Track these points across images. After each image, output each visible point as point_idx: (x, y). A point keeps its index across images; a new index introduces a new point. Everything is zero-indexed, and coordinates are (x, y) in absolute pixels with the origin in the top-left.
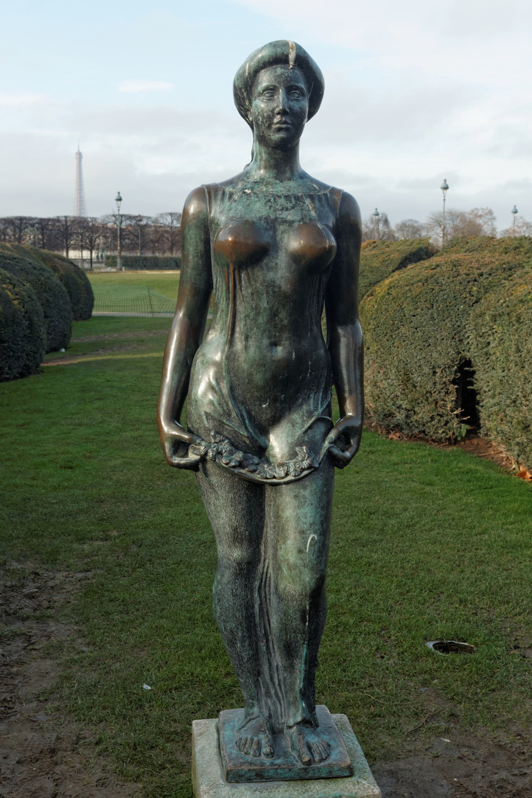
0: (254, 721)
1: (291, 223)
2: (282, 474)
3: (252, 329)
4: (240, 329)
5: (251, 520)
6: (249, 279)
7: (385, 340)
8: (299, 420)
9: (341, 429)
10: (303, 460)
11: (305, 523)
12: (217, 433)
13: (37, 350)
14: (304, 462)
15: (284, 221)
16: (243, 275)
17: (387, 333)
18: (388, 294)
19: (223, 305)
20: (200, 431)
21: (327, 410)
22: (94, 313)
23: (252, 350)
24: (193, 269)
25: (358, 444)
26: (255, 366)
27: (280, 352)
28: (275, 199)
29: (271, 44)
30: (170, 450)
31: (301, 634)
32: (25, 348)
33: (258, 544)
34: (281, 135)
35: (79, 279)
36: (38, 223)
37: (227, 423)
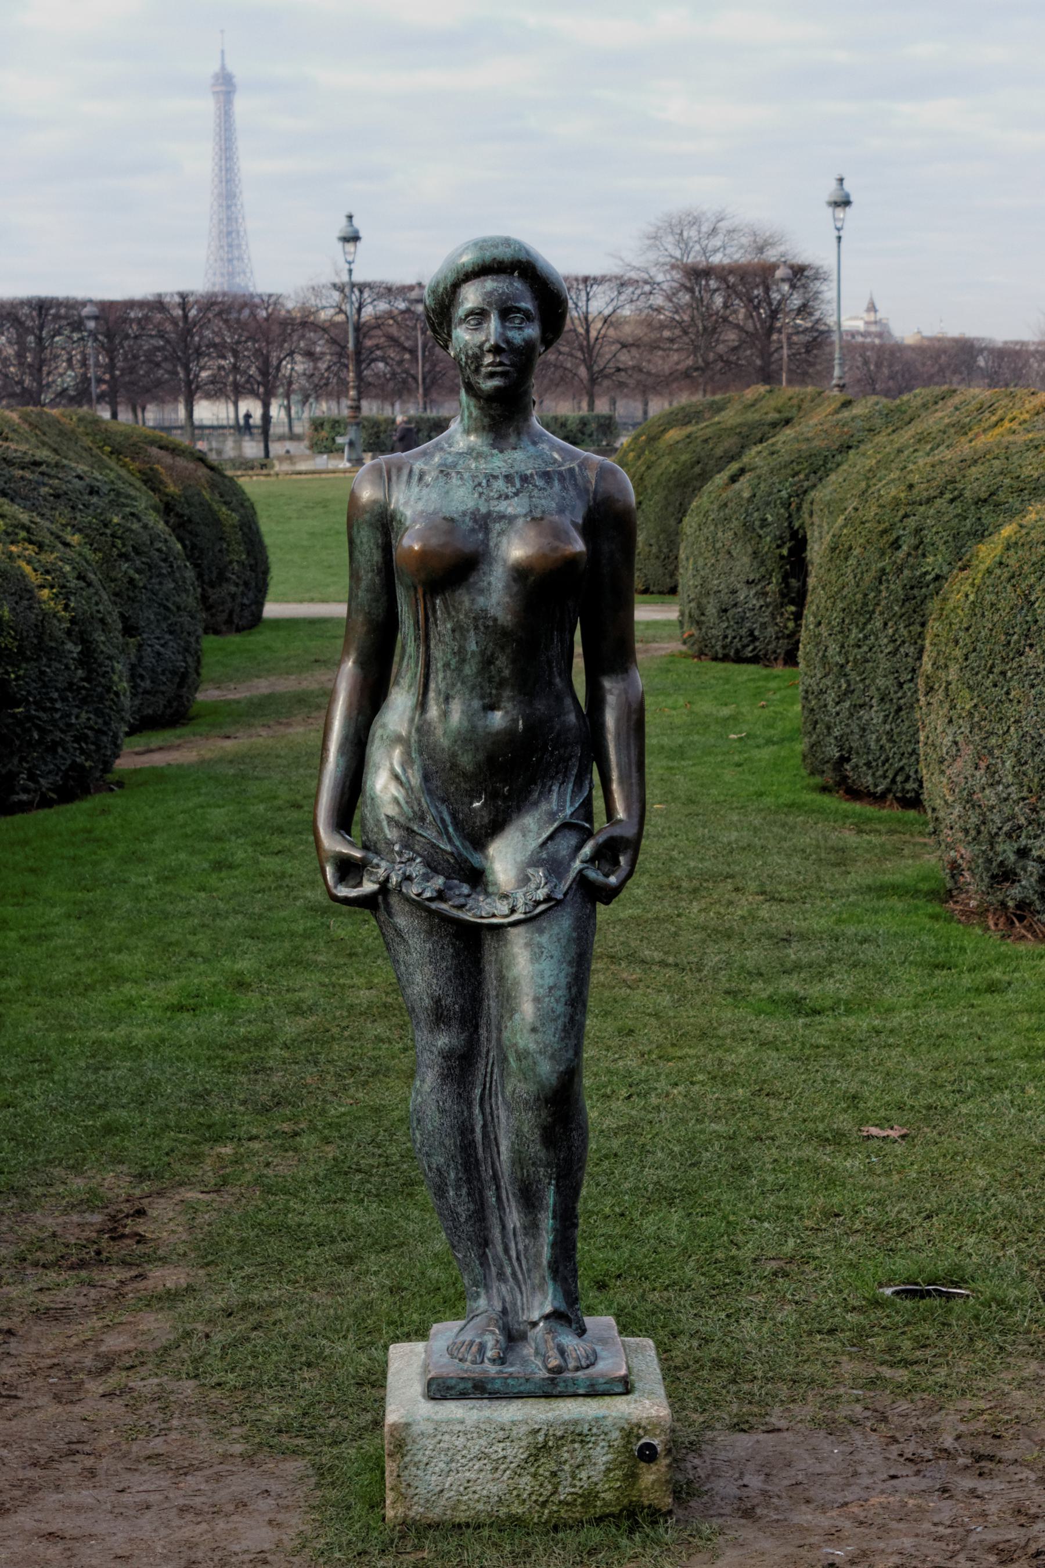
0: (479, 1319)
1: (511, 519)
2: (507, 912)
3: (454, 685)
5: (462, 985)
6: (446, 607)
7: (988, 683)
10: (538, 889)
11: (542, 986)
12: (406, 846)
13: (106, 723)
15: (502, 517)
17: (993, 666)
18: (1001, 563)
19: (411, 648)
21: (582, 811)
22: (271, 610)
23: (456, 717)
24: (367, 591)
27: (498, 719)
29: (475, 244)
30: (333, 876)
32: (73, 721)
33: (476, 1027)
34: (496, 382)
35: (224, 509)
36: (96, 318)
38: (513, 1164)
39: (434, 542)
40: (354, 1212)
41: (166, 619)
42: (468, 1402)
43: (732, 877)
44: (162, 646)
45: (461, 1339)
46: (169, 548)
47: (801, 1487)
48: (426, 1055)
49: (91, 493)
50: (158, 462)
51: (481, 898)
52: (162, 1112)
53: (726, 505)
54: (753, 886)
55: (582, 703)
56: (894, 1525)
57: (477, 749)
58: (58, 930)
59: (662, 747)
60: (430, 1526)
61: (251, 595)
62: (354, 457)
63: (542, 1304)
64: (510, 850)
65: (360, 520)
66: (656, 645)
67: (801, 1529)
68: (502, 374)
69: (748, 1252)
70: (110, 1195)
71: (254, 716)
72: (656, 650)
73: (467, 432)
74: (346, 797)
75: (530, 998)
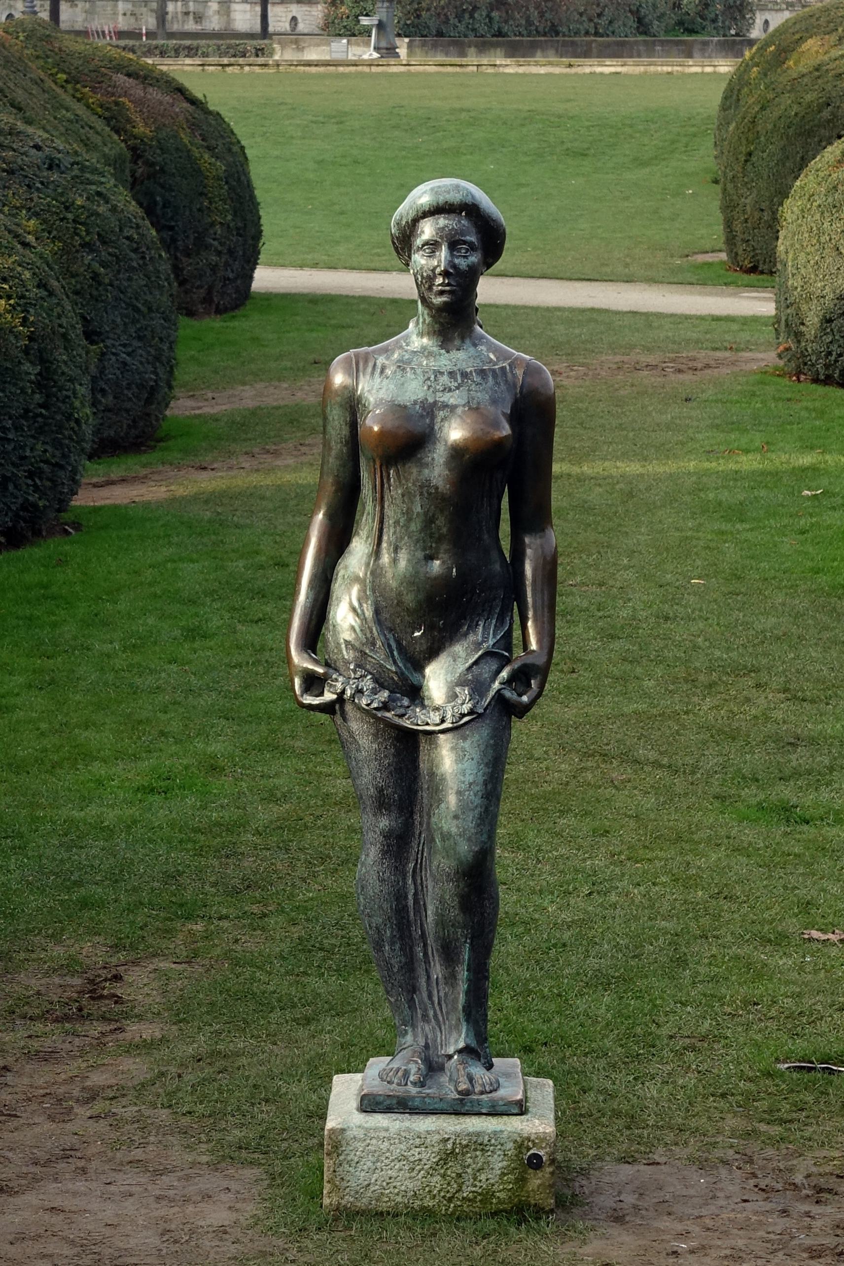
0: (405, 1051)
1: (453, 408)
2: (438, 721)
3: (402, 538)
4: (389, 538)
8: (462, 654)
9: (516, 666)
10: (463, 704)
11: (464, 782)
12: (358, 666)
13: (64, 456)
14: (464, 706)
15: (445, 406)
16: (392, 472)
20: (338, 664)
21: (503, 642)
23: (403, 564)
25: (542, 687)
26: (405, 584)
28: (436, 376)
30: (301, 686)
31: (462, 928)
32: (28, 453)
33: (412, 813)
37: (371, 654)
38: (437, 925)
39: (389, 425)
40: (314, 983)
41: (134, 321)
42: (393, 1115)
43: (756, 670)
44: (129, 354)
45: (390, 1066)
46: (142, 236)
47: (666, 1204)
48: (371, 834)
49: (50, 168)
50: (126, 94)
51: (418, 710)
52: (135, 889)
53: (835, 188)
54: (777, 682)
55: (507, 555)
56: (735, 1231)
57: (419, 591)
58: (18, 701)
59: (720, 504)
60: (358, 1212)
61: (237, 265)
62: (383, 44)
63: (457, 1041)
64: (443, 671)
65: (333, 402)
66: (747, 355)
67: (658, 1230)
68: (450, 292)
69: (665, 1031)
70: (88, 961)
71: (235, 440)
72: (747, 362)
73: (421, 335)
74: (314, 622)
75: (454, 791)
